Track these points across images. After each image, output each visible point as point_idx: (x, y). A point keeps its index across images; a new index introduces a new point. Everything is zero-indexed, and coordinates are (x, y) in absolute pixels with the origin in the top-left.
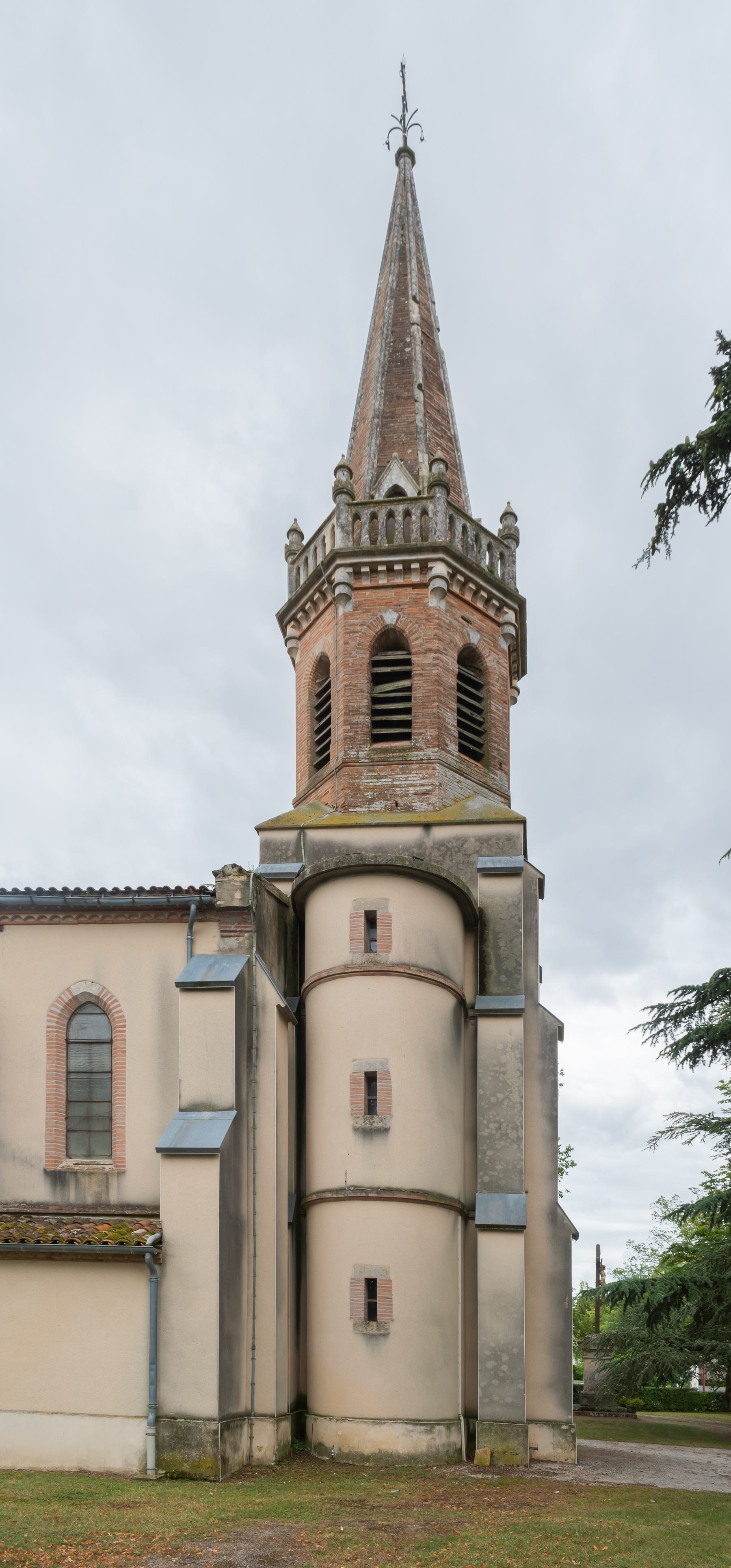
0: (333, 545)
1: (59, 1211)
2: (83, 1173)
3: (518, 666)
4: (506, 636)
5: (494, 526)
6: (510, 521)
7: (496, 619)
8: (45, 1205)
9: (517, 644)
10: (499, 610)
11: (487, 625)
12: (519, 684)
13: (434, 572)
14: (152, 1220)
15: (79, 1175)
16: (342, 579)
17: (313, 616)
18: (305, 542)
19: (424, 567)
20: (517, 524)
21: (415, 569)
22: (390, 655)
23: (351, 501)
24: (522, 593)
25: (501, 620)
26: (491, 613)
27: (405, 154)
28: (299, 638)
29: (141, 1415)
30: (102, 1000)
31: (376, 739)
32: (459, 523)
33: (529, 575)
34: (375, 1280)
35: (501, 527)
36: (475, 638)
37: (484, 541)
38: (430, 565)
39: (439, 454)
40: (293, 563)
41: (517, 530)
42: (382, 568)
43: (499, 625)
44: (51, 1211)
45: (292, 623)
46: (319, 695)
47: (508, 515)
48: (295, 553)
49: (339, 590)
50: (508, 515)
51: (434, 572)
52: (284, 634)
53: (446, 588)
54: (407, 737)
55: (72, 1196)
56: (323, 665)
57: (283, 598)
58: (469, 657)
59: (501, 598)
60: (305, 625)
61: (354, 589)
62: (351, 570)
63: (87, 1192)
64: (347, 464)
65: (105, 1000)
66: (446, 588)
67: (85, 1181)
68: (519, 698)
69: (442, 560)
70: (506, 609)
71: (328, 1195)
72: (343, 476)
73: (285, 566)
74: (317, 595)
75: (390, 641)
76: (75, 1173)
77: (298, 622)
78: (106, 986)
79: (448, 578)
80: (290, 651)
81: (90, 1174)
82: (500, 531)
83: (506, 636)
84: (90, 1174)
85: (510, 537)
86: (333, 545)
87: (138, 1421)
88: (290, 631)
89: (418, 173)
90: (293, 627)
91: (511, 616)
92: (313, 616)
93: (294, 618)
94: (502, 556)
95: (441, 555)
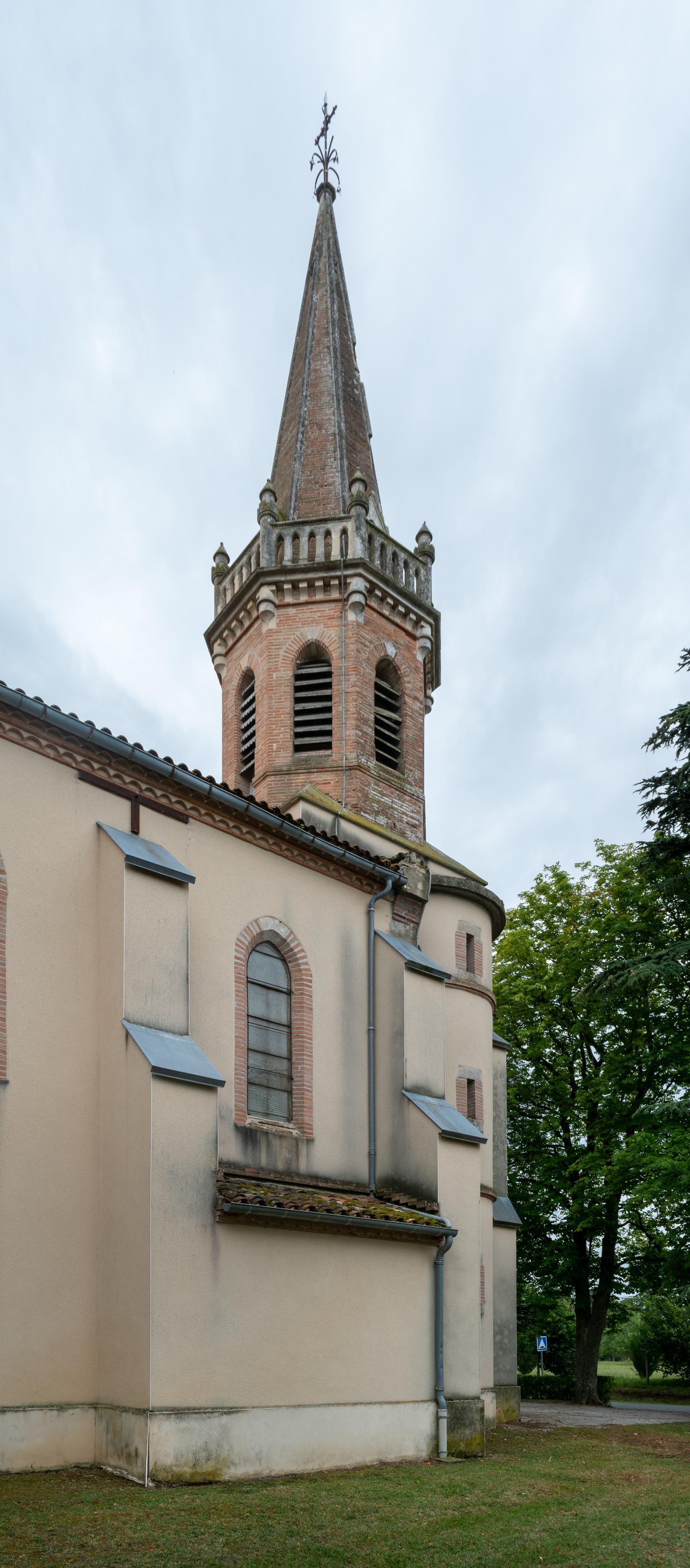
0: (258, 564)
1: (256, 1175)
2: (274, 1134)
3: (432, 676)
5: (411, 545)
6: (424, 538)
7: (413, 632)
8: (242, 1168)
9: (432, 656)
10: (417, 624)
11: (404, 639)
12: (434, 694)
13: (352, 588)
15: (271, 1137)
18: (230, 565)
19: (343, 584)
22: (313, 670)
23: (275, 523)
24: (437, 607)
25: (418, 633)
27: (326, 192)
28: (226, 655)
29: (426, 1399)
30: (288, 945)
31: (298, 749)
32: (378, 541)
33: (443, 589)
35: (417, 545)
36: (391, 651)
37: (402, 556)
38: (349, 580)
39: (358, 474)
41: (432, 548)
42: (303, 585)
43: (415, 638)
44: (248, 1174)
45: (219, 641)
47: (424, 533)
48: (220, 574)
49: (263, 607)
50: (424, 533)
51: (352, 588)
53: (363, 602)
54: (328, 746)
55: (264, 1160)
56: (248, 677)
58: (386, 670)
59: (417, 613)
60: (230, 642)
61: (278, 607)
62: (274, 588)
63: (276, 1157)
64: (271, 486)
65: (292, 945)
66: (363, 602)
67: (276, 1142)
68: (433, 707)
69: (360, 575)
70: (423, 623)
71: (372, 1172)
72: (268, 498)
74: (242, 614)
75: (313, 655)
76: (267, 1133)
77: (224, 641)
78: (295, 932)
79: (365, 592)
80: (218, 668)
81: (281, 1137)
83: (423, 648)
84: (281, 1137)
85: (426, 554)
86: (258, 564)
87: (426, 1405)
88: (217, 649)
89: (337, 206)
90: (219, 645)
91: (427, 631)
92: (239, 633)
93: (220, 636)
95: (360, 571)
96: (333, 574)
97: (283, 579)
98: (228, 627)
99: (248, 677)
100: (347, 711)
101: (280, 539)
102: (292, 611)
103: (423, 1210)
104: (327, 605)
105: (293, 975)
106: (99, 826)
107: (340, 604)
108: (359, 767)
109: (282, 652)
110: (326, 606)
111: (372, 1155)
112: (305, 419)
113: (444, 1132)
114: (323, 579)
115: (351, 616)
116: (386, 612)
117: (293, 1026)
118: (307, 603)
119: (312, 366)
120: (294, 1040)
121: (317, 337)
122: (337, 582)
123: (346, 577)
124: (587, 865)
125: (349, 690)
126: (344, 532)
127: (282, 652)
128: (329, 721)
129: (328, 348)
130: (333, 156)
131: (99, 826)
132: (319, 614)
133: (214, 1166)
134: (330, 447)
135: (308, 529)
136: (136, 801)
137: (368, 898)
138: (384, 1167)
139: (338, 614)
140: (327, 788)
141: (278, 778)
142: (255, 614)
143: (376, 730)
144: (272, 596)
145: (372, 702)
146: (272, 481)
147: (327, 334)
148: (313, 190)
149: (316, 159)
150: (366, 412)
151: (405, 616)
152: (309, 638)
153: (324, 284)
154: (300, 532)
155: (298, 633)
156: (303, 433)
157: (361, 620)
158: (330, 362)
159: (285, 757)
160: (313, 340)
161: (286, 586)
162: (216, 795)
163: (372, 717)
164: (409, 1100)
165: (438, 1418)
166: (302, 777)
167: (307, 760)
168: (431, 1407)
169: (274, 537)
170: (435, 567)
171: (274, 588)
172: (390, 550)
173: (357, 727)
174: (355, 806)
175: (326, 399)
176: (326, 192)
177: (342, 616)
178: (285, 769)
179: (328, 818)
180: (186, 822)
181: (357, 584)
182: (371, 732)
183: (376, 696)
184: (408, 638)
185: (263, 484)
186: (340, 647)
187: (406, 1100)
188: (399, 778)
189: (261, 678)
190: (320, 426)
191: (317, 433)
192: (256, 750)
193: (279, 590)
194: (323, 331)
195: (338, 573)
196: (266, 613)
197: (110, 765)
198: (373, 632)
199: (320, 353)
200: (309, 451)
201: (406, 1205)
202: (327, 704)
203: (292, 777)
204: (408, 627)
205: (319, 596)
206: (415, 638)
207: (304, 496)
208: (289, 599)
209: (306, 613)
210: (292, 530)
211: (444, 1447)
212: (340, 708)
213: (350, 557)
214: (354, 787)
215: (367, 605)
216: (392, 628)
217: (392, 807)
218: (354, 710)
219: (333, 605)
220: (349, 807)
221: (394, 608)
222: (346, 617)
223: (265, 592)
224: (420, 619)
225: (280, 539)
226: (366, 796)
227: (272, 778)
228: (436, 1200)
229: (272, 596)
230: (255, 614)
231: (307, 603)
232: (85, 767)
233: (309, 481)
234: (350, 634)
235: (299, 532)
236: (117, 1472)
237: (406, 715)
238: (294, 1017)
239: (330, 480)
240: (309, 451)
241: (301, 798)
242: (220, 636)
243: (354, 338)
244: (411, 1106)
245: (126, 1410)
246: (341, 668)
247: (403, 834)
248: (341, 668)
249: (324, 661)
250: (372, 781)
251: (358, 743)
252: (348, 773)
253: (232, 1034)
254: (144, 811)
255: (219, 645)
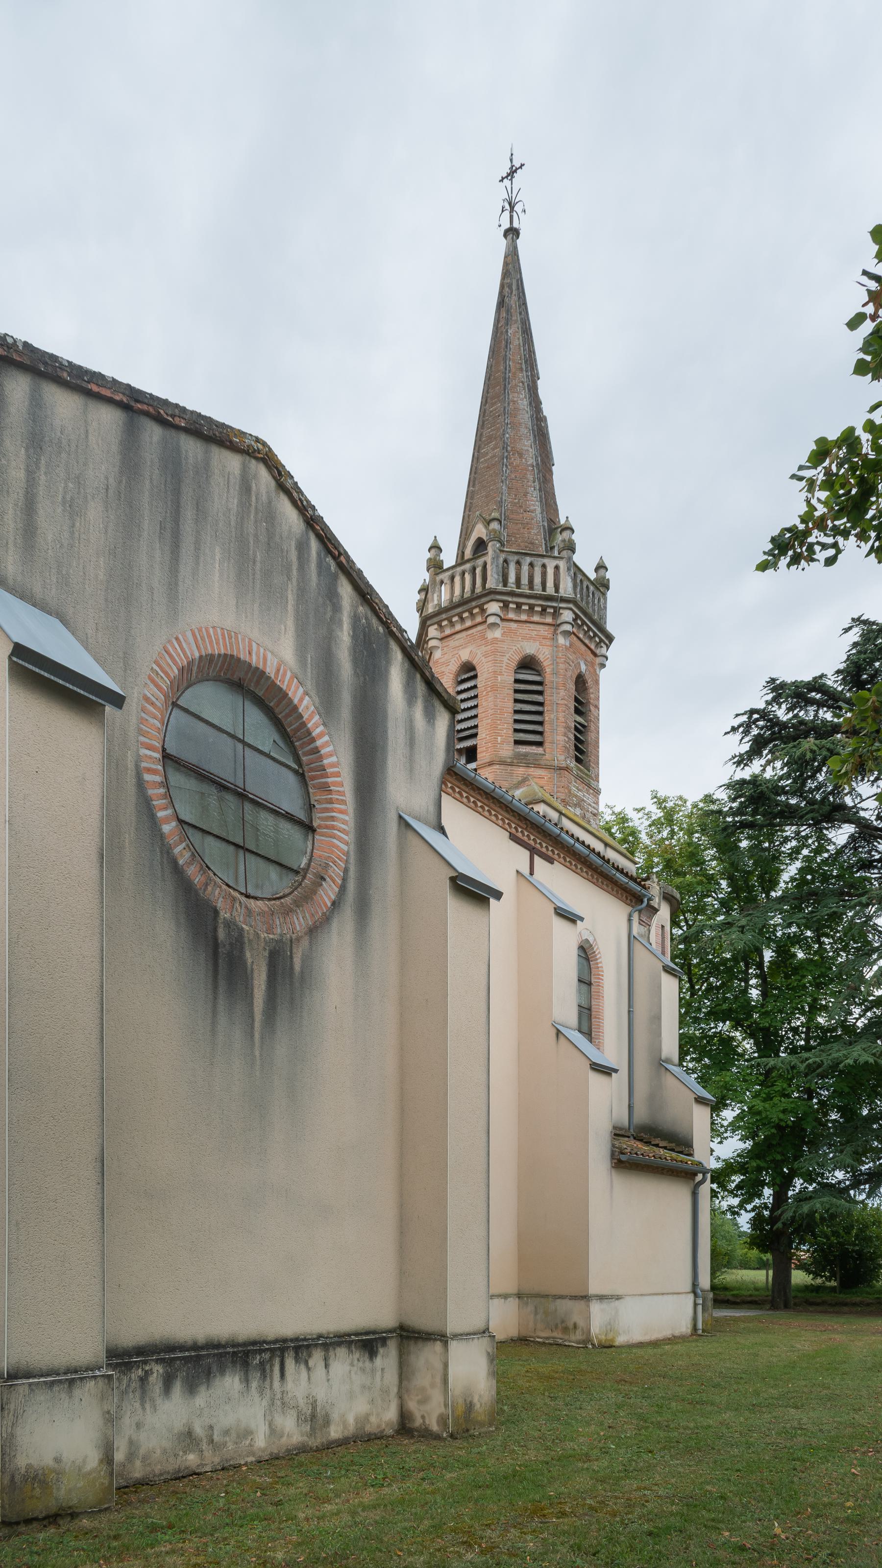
5: (592, 576)
6: (602, 571)
11: (590, 657)
19: (556, 613)
25: (598, 652)
36: (583, 668)
43: (595, 655)
50: (601, 567)
62: (502, 605)
70: (602, 644)
85: (603, 585)
96: (550, 604)
97: (510, 599)
98: (449, 620)
100: (557, 719)
102: (514, 625)
103: (681, 1152)
104: (542, 626)
105: (593, 970)
106: (517, 871)
107: (553, 628)
108: (567, 769)
109: (505, 660)
110: (541, 627)
111: (630, 1107)
112: (507, 445)
113: (595, 1064)
114: (541, 606)
115: (561, 640)
116: (581, 636)
117: (593, 1010)
118: (526, 622)
119: (511, 397)
120: (593, 1020)
121: (513, 370)
122: (552, 611)
123: (560, 608)
124: (642, 809)
125: (560, 702)
126: (557, 568)
127: (505, 660)
129: (523, 382)
131: (517, 871)
132: (535, 633)
133: (611, 1128)
134: (531, 478)
135: (528, 559)
136: (533, 851)
137: (629, 909)
138: (642, 1115)
139: (550, 636)
140: (542, 782)
141: (502, 767)
143: (575, 735)
145: (573, 712)
147: (521, 369)
150: (550, 443)
151: (591, 638)
152: (528, 651)
153: (516, 321)
154: (522, 561)
155: (518, 646)
156: (507, 457)
157: (568, 644)
158: (525, 397)
159: (507, 750)
160: (510, 371)
161: (511, 606)
162: (577, 848)
163: (572, 725)
164: (666, 1069)
165: (696, 1305)
166: (521, 769)
167: (526, 755)
168: (691, 1296)
169: (501, 560)
170: (609, 594)
171: (502, 605)
173: (565, 735)
174: (563, 801)
175: (523, 431)
176: (512, 233)
177: (554, 639)
178: (509, 760)
179: (554, 815)
180: (552, 863)
181: (567, 616)
182: (572, 737)
183: (575, 707)
184: (592, 656)
186: (553, 664)
187: (663, 1069)
188: (586, 775)
189: (485, 676)
190: (521, 455)
191: (518, 461)
193: (506, 606)
194: (518, 366)
195: (554, 604)
196: (494, 625)
197: (526, 829)
198: (574, 653)
199: (516, 386)
200: (513, 476)
201: (665, 1148)
202: (540, 709)
203: (514, 768)
204: (593, 647)
205: (536, 618)
206: (595, 655)
207: (511, 516)
208: (511, 615)
209: (525, 629)
210: (516, 558)
211: (700, 1325)
212: (552, 716)
214: (562, 784)
216: (583, 648)
217: (583, 800)
218: (563, 720)
219: (547, 628)
220: (559, 800)
221: (586, 633)
222: (557, 640)
223: (494, 607)
226: (570, 791)
227: (498, 766)
228: (692, 1147)
231: (526, 622)
232: (513, 831)
233: (514, 504)
234: (560, 655)
235: (521, 560)
236: (551, 1341)
237: (591, 721)
238: (593, 1003)
239: (532, 508)
240: (513, 476)
241: (544, 801)
243: (538, 374)
244: (668, 1074)
245: (562, 1297)
246: (553, 682)
247: (589, 822)
248: (553, 682)
249: (537, 671)
250: (573, 779)
251: (566, 747)
252: (558, 772)
254: (536, 858)
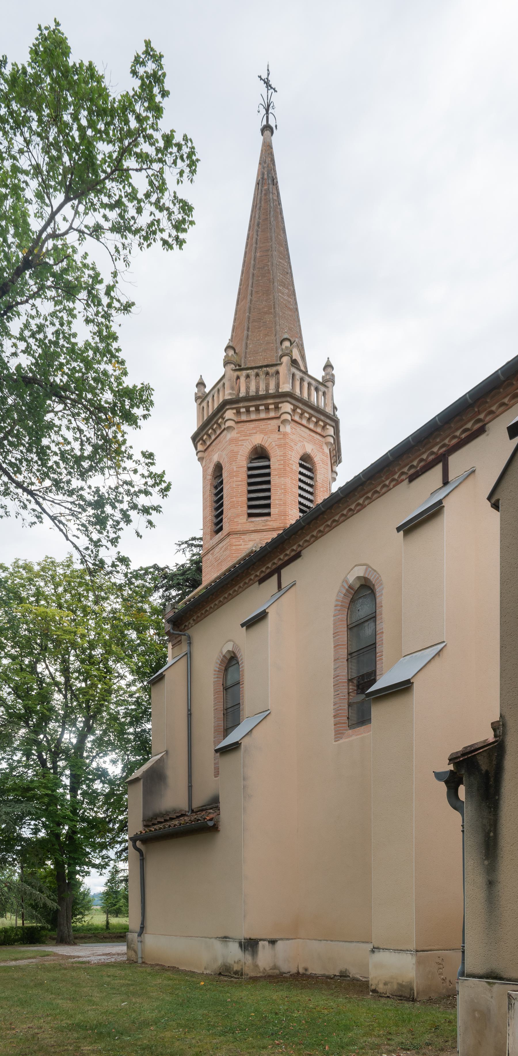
4: (327, 443)
6: (329, 370)
7: (322, 433)
10: (324, 428)
13: (282, 411)
14: (248, 371)
16: (230, 417)
17: (213, 437)
20: (333, 372)
21: (272, 409)
25: (324, 434)
26: (319, 430)
27: (267, 129)
31: (250, 515)
34: (150, 42)
38: (280, 405)
40: (200, 404)
41: (333, 375)
43: (324, 437)
45: (201, 442)
46: (216, 487)
47: (328, 366)
48: (201, 398)
50: (328, 366)
51: (282, 411)
52: (196, 448)
56: (219, 468)
57: (194, 428)
60: (208, 443)
61: (237, 423)
62: (235, 411)
64: (231, 344)
70: (328, 427)
72: (231, 352)
73: (195, 405)
75: (260, 454)
77: (204, 442)
82: (323, 377)
85: (329, 380)
89: (276, 140)
90: (201, 444)
91: (331, 431)
92: (213, 437)
94: (324, 394)
95: (289, 399)
99: (219, 468)
101: (238, 378)
128: (269, 475)
130: (272, 105)
142: (223, 427)
144: (290, 411)
146: (231, 340)
148: (260, 127)
149: (261, 107)
172: (307, 379)
185: (226, 343)
192: (224, 516)
196: (229, 428)
208: (244, 418)
213: (280, 390)
215: (292, 420)
221: (309, 420)
224: (326, 424)
225: (238, 378)
229: (290, 411)
230: (223, 427)
242: (202, 439)
253: (212, 697)
255: (201, 444)
